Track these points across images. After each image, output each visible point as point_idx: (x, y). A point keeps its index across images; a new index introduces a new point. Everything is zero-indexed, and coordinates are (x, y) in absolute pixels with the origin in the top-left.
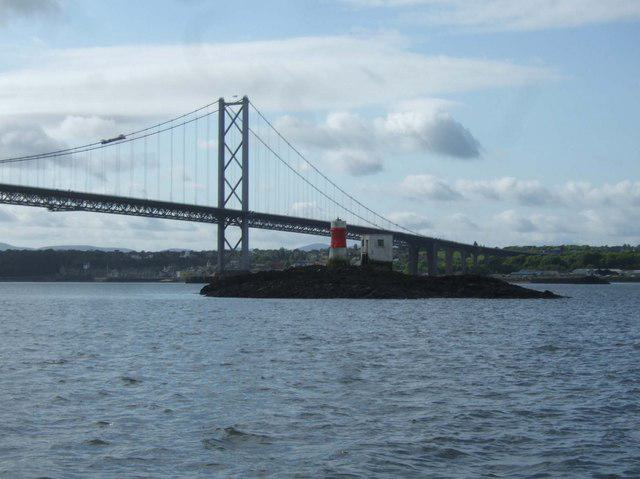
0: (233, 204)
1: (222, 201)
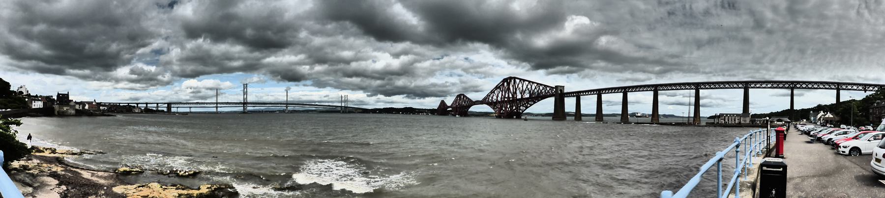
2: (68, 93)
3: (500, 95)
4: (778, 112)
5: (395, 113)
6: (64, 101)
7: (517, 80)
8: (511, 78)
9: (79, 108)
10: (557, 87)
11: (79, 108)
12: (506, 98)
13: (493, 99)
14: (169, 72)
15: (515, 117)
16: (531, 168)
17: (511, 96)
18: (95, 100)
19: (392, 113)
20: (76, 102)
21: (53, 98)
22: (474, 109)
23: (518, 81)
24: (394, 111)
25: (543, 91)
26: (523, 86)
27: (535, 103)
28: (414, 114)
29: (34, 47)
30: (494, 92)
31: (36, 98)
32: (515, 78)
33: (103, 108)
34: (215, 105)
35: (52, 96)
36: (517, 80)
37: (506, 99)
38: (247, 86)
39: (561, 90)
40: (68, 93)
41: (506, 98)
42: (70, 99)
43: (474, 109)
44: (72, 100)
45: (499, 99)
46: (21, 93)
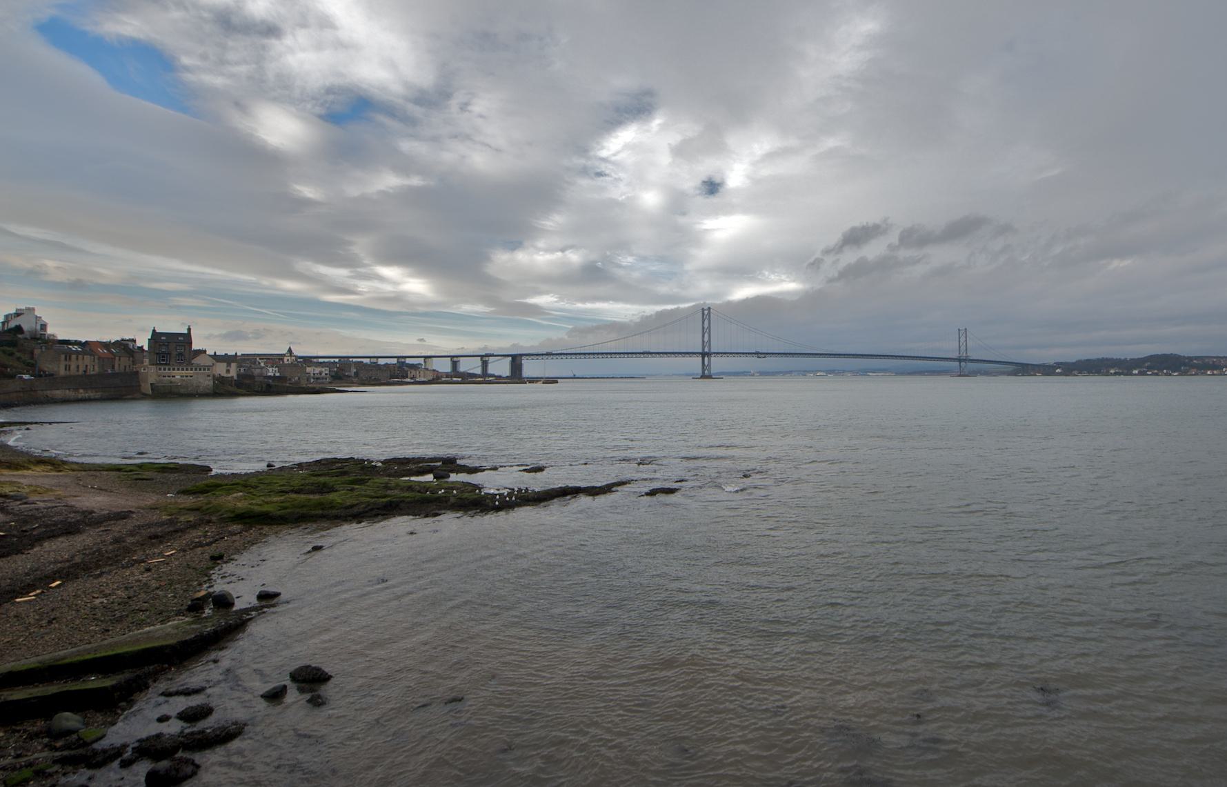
0: (706, 350)
1: (703, 349)
2: (189, 329)
4: (1120, 359)
5: (1116, 374)
6: (174, 353)
9: (228, 371)
11: (228, 371)
14: (426, 78)
15: (1136, 372)
16: (402, 750)
18: (290, 351)
19: (1108, 374)
20: (215, 357)
21: (139, 344)
24: (1112, 367)
29: (381, 118)
31: (1059, 374)
33: (317, 370)
34: (717, 364)
35: (134, 341)
38: (709, 313)
40: (189, 329)
42: (195, 347)
44: (205, 352)
46: (19, 329)
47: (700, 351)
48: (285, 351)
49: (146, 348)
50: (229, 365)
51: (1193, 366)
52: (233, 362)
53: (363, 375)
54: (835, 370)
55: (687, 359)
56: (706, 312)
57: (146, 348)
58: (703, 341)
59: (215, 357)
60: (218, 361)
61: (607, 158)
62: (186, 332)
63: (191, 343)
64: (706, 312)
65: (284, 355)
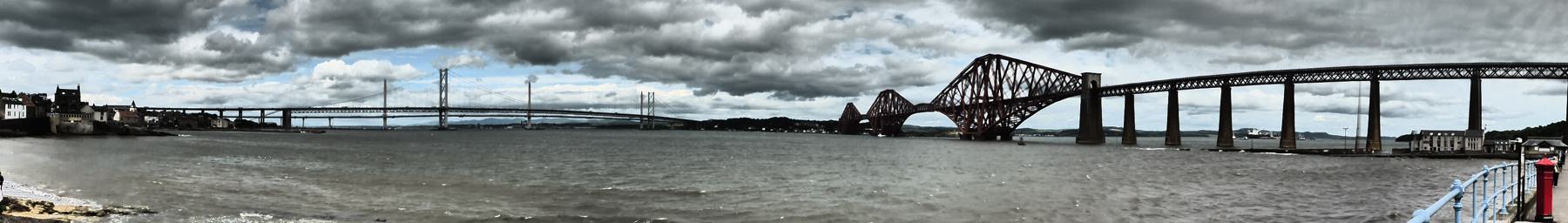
1: (441, 105)
2: (79, 87)
3: (968, 93)
5: (752, 130)
7: (1002, 61)
8: (990, 57)
9: (102, 118)
10: (1085, 76)
11: (102, 118)
12: (981, 98)
13: (955, 101)
15: (999, 137)
17: (990, 94)
18: (133, 103)
19: (747, 130)
21: (48, 98)
22: (914, 121)
23: (1005, 63)
25: (1057, 83)
26: (1015, 74)
27: (1040, 108)
28: (791, 131)
30: (956, 86)
32: (999, 57)
33: (151, 119)
35: (45, 95)
36: (1002, 61)
37: (981, 101)
39: (1094, 83)
40: (79, 87)
41: (981, 98)
43: (914, 121)
44: (87, 103)
45: (967, 101)
47: (382, 106)
48: (130, 104)
49: (53, 100)
50: (102, 114)
51: (797, 127)
52: (1009, 100)
53: (181, 122)
54: (537, 129)
55: (378, 119)
56: (443, 73)
57: (53, 100)
58: (441, 98)
59: (95, 108)
60: (96, 111)
61: (495, 60)
62: (76, 88)
63: (1563, 122)
64: (443, 73)
65: (130, 107)
